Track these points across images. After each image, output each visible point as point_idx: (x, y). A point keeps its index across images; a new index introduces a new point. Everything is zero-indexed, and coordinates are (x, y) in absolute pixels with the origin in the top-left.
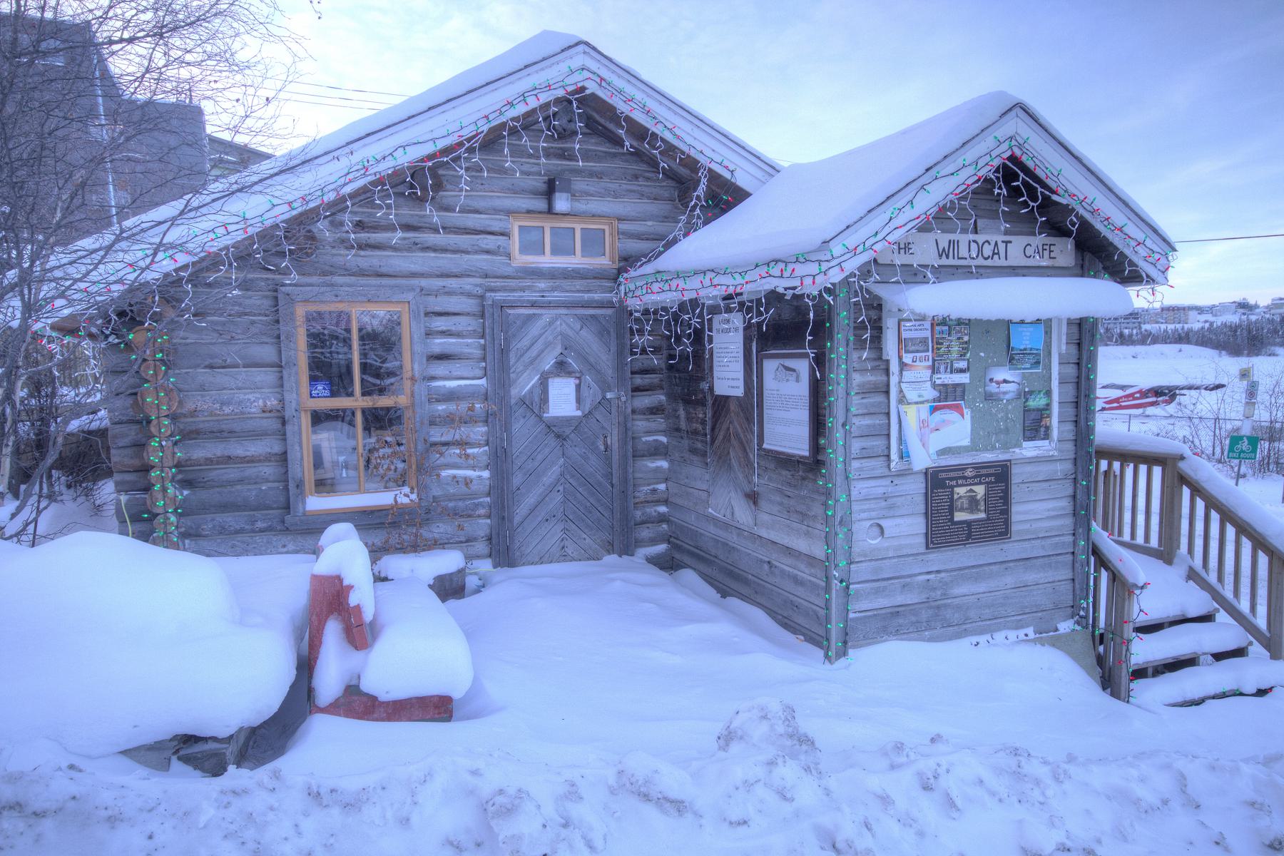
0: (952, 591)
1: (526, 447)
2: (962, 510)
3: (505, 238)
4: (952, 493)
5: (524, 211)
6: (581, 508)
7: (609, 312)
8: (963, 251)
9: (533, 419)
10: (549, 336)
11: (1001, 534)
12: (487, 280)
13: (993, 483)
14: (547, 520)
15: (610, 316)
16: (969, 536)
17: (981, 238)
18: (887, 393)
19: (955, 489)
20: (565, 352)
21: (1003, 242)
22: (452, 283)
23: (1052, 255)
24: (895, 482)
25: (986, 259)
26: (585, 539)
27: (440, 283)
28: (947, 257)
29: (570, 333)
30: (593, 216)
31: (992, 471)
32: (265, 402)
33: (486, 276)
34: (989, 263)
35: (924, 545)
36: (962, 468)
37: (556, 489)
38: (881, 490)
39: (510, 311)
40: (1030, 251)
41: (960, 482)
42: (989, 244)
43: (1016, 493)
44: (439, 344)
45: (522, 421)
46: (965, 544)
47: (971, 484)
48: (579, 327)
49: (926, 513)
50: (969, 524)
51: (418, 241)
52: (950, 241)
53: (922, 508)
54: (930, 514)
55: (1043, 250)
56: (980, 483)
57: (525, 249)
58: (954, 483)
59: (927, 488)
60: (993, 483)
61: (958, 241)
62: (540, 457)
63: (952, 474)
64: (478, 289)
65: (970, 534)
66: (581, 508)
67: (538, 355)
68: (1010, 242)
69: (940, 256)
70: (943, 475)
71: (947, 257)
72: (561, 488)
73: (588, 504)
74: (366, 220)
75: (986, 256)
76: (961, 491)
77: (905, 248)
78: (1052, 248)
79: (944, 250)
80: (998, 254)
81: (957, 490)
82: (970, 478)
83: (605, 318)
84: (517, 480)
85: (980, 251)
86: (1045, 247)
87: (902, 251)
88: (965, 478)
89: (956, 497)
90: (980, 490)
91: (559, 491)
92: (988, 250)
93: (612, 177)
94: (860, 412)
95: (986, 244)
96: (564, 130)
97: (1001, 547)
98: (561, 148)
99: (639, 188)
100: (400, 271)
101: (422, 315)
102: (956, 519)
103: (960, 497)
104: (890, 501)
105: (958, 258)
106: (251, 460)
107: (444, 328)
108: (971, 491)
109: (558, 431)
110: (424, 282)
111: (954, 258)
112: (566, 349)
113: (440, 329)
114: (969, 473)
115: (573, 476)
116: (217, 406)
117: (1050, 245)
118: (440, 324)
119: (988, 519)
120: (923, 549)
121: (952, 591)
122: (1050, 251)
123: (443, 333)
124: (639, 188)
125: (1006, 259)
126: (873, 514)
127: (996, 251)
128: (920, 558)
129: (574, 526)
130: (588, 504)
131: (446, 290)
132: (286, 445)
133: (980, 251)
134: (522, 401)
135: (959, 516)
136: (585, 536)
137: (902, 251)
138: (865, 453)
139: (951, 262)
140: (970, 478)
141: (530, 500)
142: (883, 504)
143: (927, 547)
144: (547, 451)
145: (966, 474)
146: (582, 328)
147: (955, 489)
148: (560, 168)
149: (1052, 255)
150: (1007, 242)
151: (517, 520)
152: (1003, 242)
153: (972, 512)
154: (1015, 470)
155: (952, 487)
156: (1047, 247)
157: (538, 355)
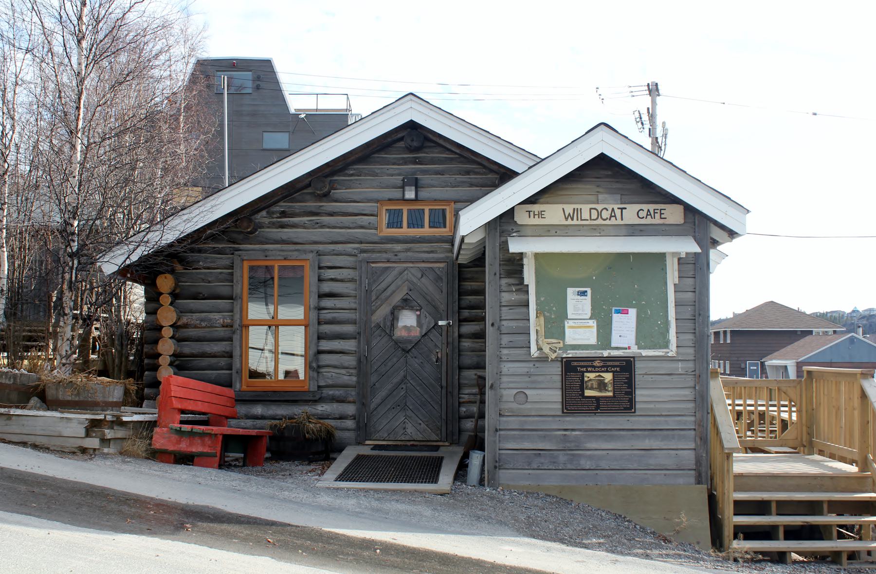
0: (585, 445)
1: (380, 356)
2: (592, 388)
3: (375, 217)
4: (583, 377)
5: (387, 199)
6: (418, 402)
7: (442, 265)
8: (585, 215)
9: (386, 339)
10: (399, 282)
11: (626, 409)
12: (363, 245)
13: (618, 372)
14: (394, 408)
15: (443, 268)
16: (597, 408)
17: (600, 207)
18: (528, 305)
19: (586, 374)
20: (410, 293)
21: (619, 208)
22: (339, 247)
23: (663, 216)
24: (536, 366)
25: (604, 220)
26: (420, 424)
27: (332, 247)
28: (572, 219)
29: (415, 280)
30: (435, 200)
31: (617, 363)
32: (223, 320)
33: (361, 243)
34: (607, 222)
35: (561, 410)
36: (591, 359)
37: (401, 386)
38: (526, 370)
39: (373, 265)
40: (641, 214)
41: (589, 369)
42: (607, 210)
43: (639, 380)
44: (327, 287)
45: (379, 338)
46: (595, 413)
47: (598, 372)
48: (420, 276)
49: (562, 388)
50: (597, 399)
51: (318, 221)
52: (574, 209)
53: (559, 385)
54: (565, 389)
55: (654, 213)
56: (607, 371)
57: (390, 225)
58: (584, 369)
59: (562, 371)
60: (618, 372)
61: (581, 209)
62: (390, 364)
63: (582, 364)
64: (355, 251)
65: (597, 406)
66: (418, 402)
67: (392, 294)
68: (625, 208)
69: (567, 219)
70: (575, 364)
71: (572, 219)
72: (404, 386)
73: (423, 399)
74: (287, 210)
75: (604, 217)
76: (592, 376)
77: (539, 215)
78: (662, 212)
79: (569, 214)
80: (615, 216)
81: (586, 374)
82: (598, 367)
83: (439, 269)
84: (373, 379)
85: (599, 214)
86: (656, 211)
87: (536, 216)
88: (594, 367)
89: (586, 379)
90: (608, 377)
91: (402, 388)
92: (605, 214)
93: (451, 174)
94: (268, 282)
95: (605, 210)
96: (411, 146)
97: (628, 418)
98: (414, 157)
99: (469, 180)
100: (306, 241)
101: (317, 268)
102: (586, 394)
103: (590, 380)
104: (533, 378)
105: (581, 220)
106: (214, 356)
107: (333, 277)
108: (600, 376)
109: (405, 348)
110: (321, 247)
111: (577, 220)
112: (410, 290)
113: (330, 277)
114: (596, 363)
115: (413, 379)
116: (198, 322)
117: (661, 210)
118: (331, 274)
119: (614, 396)
120: (560, 413)
121: (585, 445)
122: (661, 214)
123: (332, 280)
124: (469, 180)
125: (622, 220)
126: (519, 385)
127: (613, 214)
128: (558, 419)
129: (413, 415)
130: (423, 399)
131: (335, 252)
132: (232, 347)
133: (599, 214)
134: (378, 326)
135: (588, 393)
136: (421, 422)
137: (536, 216)
138: (511, 345)
139: (575, 222)
140: (598, 367)
141: (382, 393)
142: (527, 379)
143: (563, 412)
144: (395, 360)
145: (595, 364)
146: (422, 276)
147: (586, 374)
148: (413, 170)
149: (663, 216)
150: (622, 209)
151: (373, 406)
152: (619, 208)
153: (600, 391)
154: (638, 365)
155: (584, 372)
156: (658, 211)
157: (392, 294)
